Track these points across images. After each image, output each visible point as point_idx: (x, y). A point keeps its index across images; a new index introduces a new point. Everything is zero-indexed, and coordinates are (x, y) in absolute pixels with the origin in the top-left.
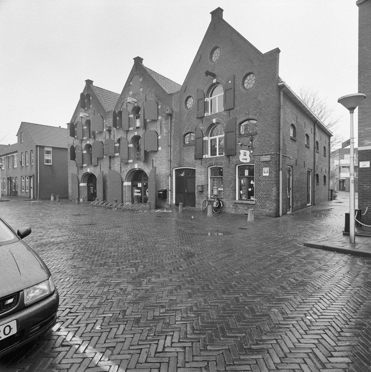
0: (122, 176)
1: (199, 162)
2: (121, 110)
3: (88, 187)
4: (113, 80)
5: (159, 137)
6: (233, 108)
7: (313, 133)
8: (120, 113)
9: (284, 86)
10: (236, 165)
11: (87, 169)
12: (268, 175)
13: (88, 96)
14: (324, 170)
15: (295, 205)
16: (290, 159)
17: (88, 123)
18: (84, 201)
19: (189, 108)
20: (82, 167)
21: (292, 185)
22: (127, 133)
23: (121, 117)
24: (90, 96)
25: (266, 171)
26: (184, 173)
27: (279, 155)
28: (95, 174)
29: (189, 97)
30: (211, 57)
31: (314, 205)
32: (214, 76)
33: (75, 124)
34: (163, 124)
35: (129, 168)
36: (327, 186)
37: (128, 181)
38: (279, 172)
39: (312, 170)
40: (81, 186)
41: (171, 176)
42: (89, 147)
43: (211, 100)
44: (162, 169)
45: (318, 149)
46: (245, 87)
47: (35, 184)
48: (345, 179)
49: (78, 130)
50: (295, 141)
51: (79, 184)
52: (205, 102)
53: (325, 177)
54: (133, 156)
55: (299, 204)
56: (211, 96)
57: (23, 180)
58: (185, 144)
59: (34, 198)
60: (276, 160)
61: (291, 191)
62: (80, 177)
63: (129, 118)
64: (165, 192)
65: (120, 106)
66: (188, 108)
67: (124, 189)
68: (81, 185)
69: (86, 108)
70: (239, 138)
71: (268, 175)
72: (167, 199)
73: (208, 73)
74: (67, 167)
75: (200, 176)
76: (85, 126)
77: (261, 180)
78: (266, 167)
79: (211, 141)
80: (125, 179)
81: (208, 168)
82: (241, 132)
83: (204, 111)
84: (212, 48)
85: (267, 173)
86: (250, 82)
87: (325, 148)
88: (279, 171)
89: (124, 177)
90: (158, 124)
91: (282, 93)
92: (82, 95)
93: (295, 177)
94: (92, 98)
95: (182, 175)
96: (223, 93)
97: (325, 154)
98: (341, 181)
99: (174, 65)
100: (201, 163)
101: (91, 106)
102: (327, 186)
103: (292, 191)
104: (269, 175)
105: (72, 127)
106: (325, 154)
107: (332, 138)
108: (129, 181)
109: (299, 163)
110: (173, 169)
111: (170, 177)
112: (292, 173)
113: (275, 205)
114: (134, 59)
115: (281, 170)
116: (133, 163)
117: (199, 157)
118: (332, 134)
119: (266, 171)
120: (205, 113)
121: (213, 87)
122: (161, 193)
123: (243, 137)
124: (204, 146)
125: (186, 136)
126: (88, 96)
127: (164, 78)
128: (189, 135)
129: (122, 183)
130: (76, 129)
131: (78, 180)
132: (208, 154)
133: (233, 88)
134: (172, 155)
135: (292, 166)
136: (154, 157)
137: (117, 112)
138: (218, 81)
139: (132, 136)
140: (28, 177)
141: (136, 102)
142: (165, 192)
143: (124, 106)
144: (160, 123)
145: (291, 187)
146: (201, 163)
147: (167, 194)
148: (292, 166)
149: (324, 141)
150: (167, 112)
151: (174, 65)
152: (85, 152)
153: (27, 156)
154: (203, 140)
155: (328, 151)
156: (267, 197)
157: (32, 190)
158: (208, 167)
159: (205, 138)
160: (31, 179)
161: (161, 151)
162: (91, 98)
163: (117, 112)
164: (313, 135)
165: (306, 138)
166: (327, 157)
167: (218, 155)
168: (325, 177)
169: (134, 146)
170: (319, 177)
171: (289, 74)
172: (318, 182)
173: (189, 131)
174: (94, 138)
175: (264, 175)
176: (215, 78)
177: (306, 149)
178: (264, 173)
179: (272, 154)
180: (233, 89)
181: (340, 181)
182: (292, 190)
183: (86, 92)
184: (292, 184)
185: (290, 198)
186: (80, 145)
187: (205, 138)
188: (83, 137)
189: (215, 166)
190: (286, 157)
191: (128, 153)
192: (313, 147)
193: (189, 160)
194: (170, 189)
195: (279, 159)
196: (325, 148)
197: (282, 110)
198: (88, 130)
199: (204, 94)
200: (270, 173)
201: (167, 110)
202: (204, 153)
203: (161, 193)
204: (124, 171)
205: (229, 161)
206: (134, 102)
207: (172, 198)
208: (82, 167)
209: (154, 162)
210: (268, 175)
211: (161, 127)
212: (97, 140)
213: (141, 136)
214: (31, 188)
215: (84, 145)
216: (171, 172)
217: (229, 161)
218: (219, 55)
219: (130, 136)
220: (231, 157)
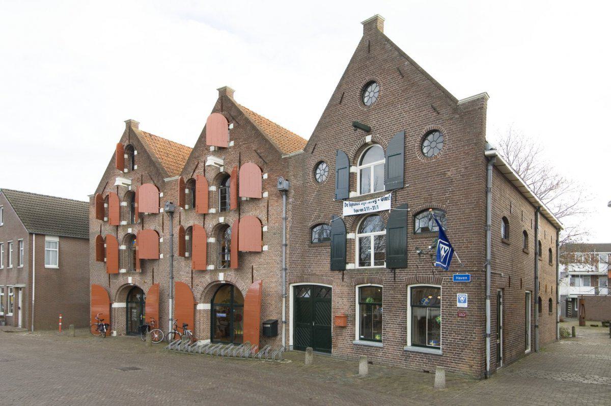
0: (195, 294)
1: (338, 275)
2: (195, 177)
3: (128, 310)
4: (180, 123)
5: (265, 229)
6: (402, 188)
7: (533, 227)
8: (193, 182)
9: (494, 156)
10: (407, 286)
11: (127, 278)
12: (466, 306)
13: (131, 149)
14: (549, 290)
15: (508, 355)
16: (501, 277)
17: (132, 196)
18: (119, 334)
19: (319, 181)
20: (117, 274)
21: (503, 321)
22: (204, 219)
23: (193, 190)
24: (132, 150)
25: (462, 298)
26: (309, 292)
27: (486, 272)
28: (142, 288)
29: (321, 162)
30: (362, 96)
31: (535, 351)
32: (368, 131)
33: (104, 197)
34: (272, 205)
35: (207, 279)
36: (554, 316)
37: (204, 302)
38: (485, 301)
39: (532, 291)
40: (115, 308)
41: (286, 297)
42: (131, 238)
43: (361, 171)
44: (270, 282)
45: (540, 255)
46: (423, 154)
47: (27, 304)
48: (576, 297)
49: (112, 208)
50: (509, 245)
51: (111, 305)
52: (350, 173)
53: (550, 300)
54: (215, 258)
55: (514, 353)
56: (361, 164)
57: (12, 294)
58: (312, 243)
59: (24, 326)
60: (481, 282)
61: (501, 331)
62: (113, 291)
63: (209, 192)
64: (275, 324)
65: (190, 170)
66: (318, 182)
67: (198, 315)
68: (116, 305)
69: (126, 170)
70: (412, 239)
71: (465, 305)
72: (279, 337)
73: (356, 126)
74: (89, 272)
75: (340, 301)
76: (124, 201)
77: (453, 315)
78: (462, 291)
79: (361, 240)
80: (201, 299)
81: (355, 288)
82: (416, 229)
83: (349, 189)
84: (364, 82)
85: (465, 302)
86: (372, 94)
87: (550, 250)
88: (486, 299)
89: (198, 296)
90: (263, 204)
91: (491, 168)
92: (120, 146)
93: (507, 305)
94: (138, 153)
95: (307, 296)
96: (384, 161)
97: (551, 261)
98: (570, 301)
99: (295, 106)
100: (343, 278)
101: (136, 167)
102: (554, 316)
103: (503, 332)
104: (468, 306)
105: (100, 200)
106: (551, 261)
107: (562, 232)
108: (207, 303)
109: (513, 281)
110: (289, 284)
111: (284, 299)
112: (503, 300)
113: (478, 357)
114: (218, 90)
115: (488, 298)
116: (216, 271)
117: (338, 264)
118: (562, 226)
119: (462, 298)
120: (349, 191)
121: (363, 150)
122: (269, 326)
123: (419, 238)
124: (348, 249)
125: (315, 230)
126: (131, 149)
127: (269, 123)
128: (318, 228)
129: (195, 305)
130: (106, 205)
131: (110, 297)
132: (354, 263)
133: (402, 152)
134: (288, 259)
135: (503, 289)
136: (255, 262)
137: (185, 180)
138: (375, 140)
139: (214, 223)
140: (11, 289)
141: (221, 166)
142: (275, 324)
143: (200, 171)
144: (266, 204)
145: (501, 325)
146: (343, 278)
147: (279, 328)
148: (503, 289)
149: (550, 239)
150: (280, 187)
151: (295, 106)
152: (123, 247)
153: (11, 250)
154: (346, 239)
155: (555, 255)
156: (464, 344)
157: (20, 312)
158: (355, 286)
159: (350, 236)
160: (18, 293)
161: (268, 252)
162: (136, 153)
163: (185, 180)
164: (533, 230)
165: (503, 224)
166: (555, 266)
167: (373, 266)
168: (550, 300)
169: (218, 240)
170: (543, 302)
171: (497, 135)
172: (540, 310)
173: (319, 221)
174: (142, 222)
175: (459, 305)
176: (369, 135)
177: (525, 255)
178: (460, 302)
179: (473, 271)
180: (403, 154)
181: (567, 301)
182: (503, 330)
183: (127, 142)
184: (503, 319)
185: (499, 344)
186: (114, 234)
187: (350, 236)
188: (120, 220)
189: (369, 285)
190: (496, 273)
191: (207, 253)
192: (533, 251)
193: (320, 271)
194: (284, 319)
195: (486, 279)
196: (550, 250)
197: (490, 196)
198: (129, 209)
199: (349, 159)
200: (470, 302)
201: (280, 183)
202: (347, 261)
203: (269, 326)
204: (197, 285)
205: (395, 277)
206: (218, 164)
207: (287, 336)
208: (117, 274)
209: (254, 271)
210: (466, 306)
211: (268, 211)
212: (146, 226)
213: (231, 225)
214: (19, 308)
215: (121, 235)
216: (287, 290)
217: (395, 277)
218: (376, 95)
219: (210, 224)
220: (397, 271)
